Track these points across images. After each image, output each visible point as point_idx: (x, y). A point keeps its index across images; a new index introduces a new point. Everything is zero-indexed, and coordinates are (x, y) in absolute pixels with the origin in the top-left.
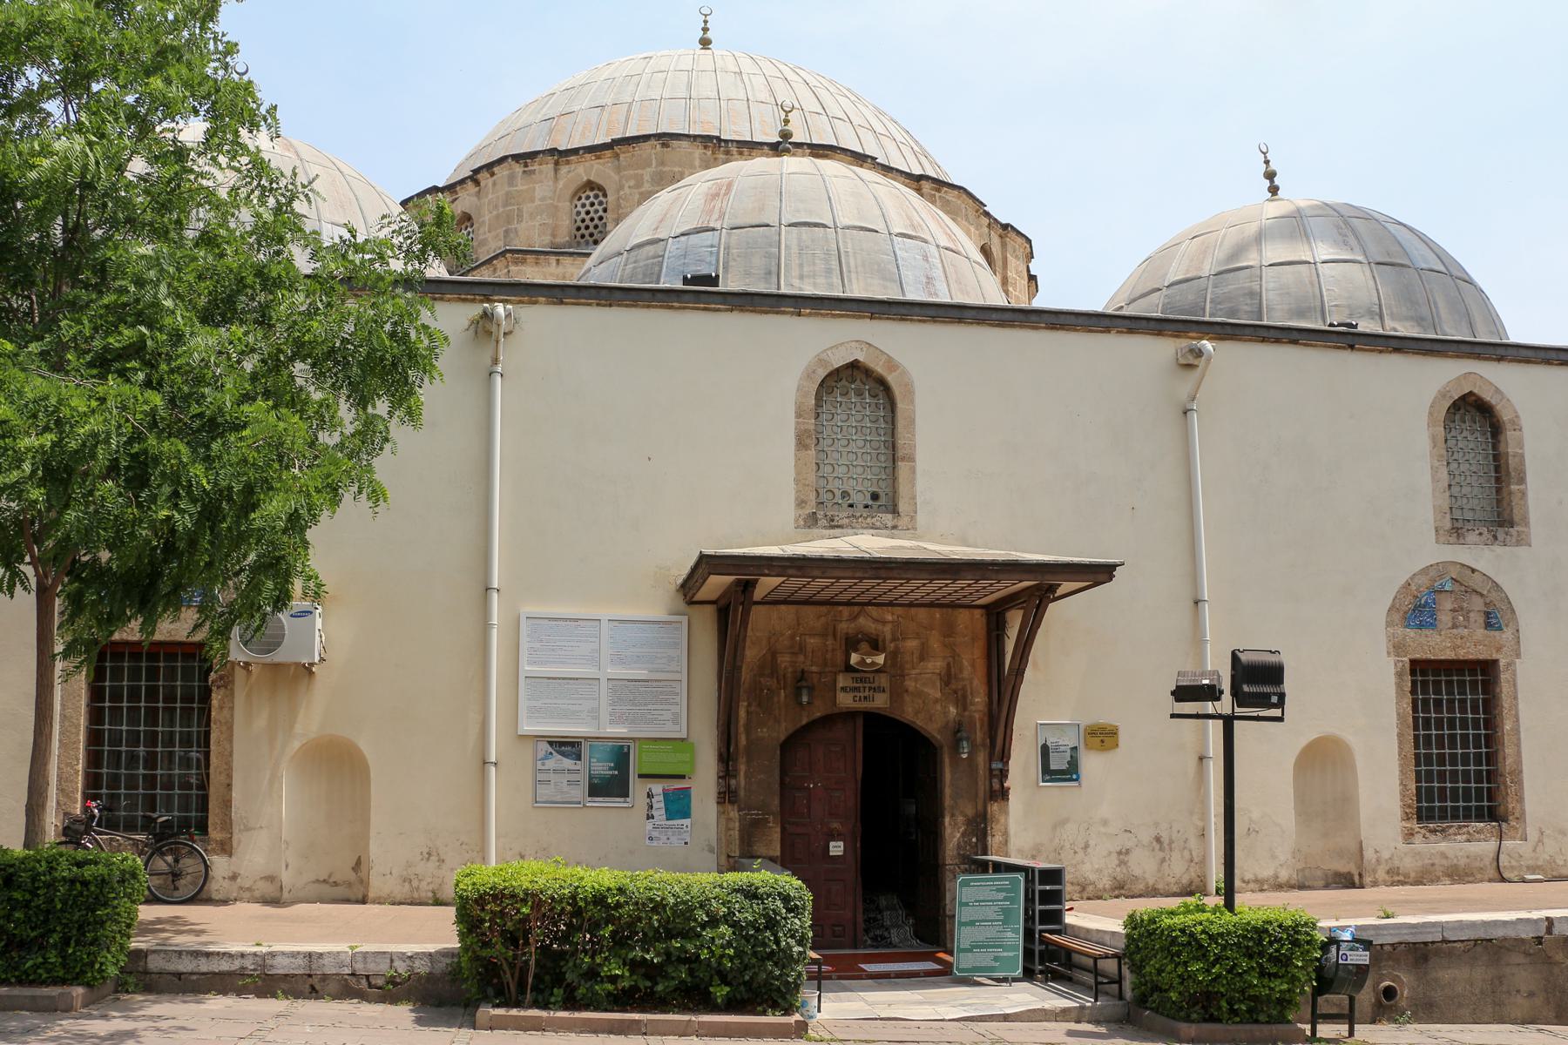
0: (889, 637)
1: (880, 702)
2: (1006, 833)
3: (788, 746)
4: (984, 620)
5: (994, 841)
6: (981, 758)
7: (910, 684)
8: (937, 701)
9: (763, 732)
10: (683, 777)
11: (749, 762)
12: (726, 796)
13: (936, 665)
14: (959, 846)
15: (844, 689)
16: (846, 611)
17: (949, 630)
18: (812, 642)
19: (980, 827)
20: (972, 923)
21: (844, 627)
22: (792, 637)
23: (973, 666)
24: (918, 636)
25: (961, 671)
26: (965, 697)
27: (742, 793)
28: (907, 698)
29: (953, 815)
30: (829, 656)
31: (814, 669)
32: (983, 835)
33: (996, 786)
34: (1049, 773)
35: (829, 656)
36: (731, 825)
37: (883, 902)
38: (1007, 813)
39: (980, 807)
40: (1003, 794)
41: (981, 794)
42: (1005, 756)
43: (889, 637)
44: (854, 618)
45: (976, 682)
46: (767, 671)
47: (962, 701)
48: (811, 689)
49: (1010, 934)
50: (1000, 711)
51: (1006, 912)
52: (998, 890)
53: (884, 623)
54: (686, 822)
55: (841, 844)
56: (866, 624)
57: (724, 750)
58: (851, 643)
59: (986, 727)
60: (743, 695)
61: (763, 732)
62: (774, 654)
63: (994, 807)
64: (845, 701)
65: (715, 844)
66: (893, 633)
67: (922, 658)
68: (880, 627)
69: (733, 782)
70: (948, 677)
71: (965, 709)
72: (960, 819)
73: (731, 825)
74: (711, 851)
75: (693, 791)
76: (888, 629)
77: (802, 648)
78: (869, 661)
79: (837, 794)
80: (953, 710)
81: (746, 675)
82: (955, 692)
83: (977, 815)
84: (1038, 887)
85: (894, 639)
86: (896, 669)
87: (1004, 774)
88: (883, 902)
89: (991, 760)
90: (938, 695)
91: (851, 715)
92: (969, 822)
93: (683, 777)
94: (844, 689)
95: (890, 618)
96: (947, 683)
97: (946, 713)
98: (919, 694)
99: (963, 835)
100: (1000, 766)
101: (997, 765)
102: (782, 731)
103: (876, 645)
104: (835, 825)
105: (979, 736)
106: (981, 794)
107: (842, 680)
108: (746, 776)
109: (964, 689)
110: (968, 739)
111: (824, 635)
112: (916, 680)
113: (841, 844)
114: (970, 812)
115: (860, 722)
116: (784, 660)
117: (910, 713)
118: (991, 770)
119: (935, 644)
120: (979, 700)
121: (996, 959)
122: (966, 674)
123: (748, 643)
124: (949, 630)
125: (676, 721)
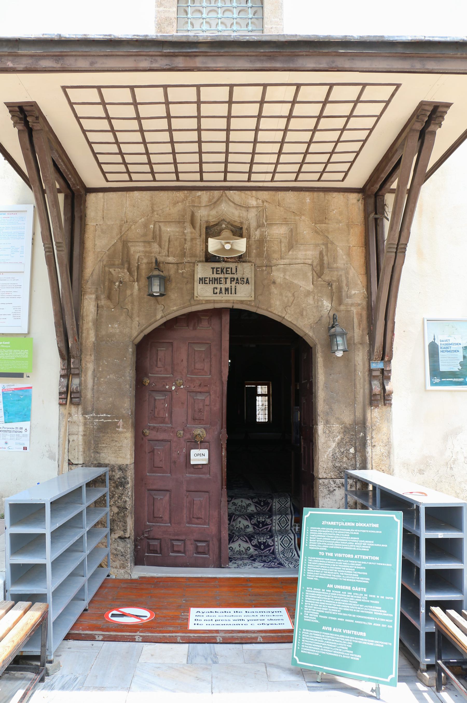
0: (253, 224)
1: (243, 296)
2: (388, 444)
3: (145, 346)
4: (360, 205)
5: (374, 453)
6: (360, 357)
7: (278, 275)
8: (308, 294)
9: (114, 328)
10: (20, 375)
11: (98, 360)
12: (69, 397)
13: (307, 254)
14: (334, 458)
15: (202, 280)
16: (204, 196)
17: (321, 216)
18: (169, 230)
19: (358, 438)
20: (321, 584)
21: (204, 214)
22: (146, 225)
23: (349, 255)
24: (285, 221)
25: (335, 259)
26: (340, 289)
27: (89, 394)
28: (274, 290)
29: (327, 422)
30: (187, 246)
31: (171, 259)
32: (362, 445)
33: (377, 388)
34: (438, 375)
35: (187, 246)
36: (74, 429)
37: (276, 504)
38: (389, 420)
39: (359, 414)
40: (385, 398)
41: (360, 398)
42: (385, 354)
43: (253, 224)
44: (214, 204)
45: (352, 272)
46: (118, 261)
47: (337, 293)
48: (165, 281)
49: (378, 610)
50: (378, 298)
51: (373, 572)
52: (363, 537)
53: (248, 208)
54: (25, 425)
55: (206, 452)
56: (228, 210)
57: (63, 345)
58: (212, 230)
59: (365, 322)
60: (89, 287)
61: (114, 328)
62: (125, 243)
63: (374, 414)
64: (205, 295)
65: (55, 449)
66: (258, 218)
67: (291, 247)
68: (244, 213)
69: (75, 382)
70: (320, 268)
71: (340, 302)
72: (336, 427)
73: (74, 429)
74: (52, 457)
75: (34, 393)
76: (252, 214)
77: (157, 237)
78: (228, 247)
79: (200, 397)
80: (327, 304)
81: (92, 265)
82: (330, 284)
83: (355, 423)
84: (425, 534)
85: (259, 226)
86: (260, 253)
87: (385, 375)
88: (276, 504)
89: (370, 360)
90: (310, 287)
91: (216, 313)
92: (346, 430)
93: (20, 375)
94: (202, 280)
95: (253, 202)
96: (320, 275)
97: (319, 307)
98: (289, 286)
99: (339, 445)
100: (380, 365)
101: (377, 365)
102: (134, 327)
103: (238, 232)
104: (199, 431)
105: (358, 333)
106: (360, 398)
107: (203, 270)
108: (94, 376)
109: (339, 281)
110: (343, 335)
111: (180, 222)
112: (285, 271)
113: (206, 452)
114: (348, 419)
115: (226, 319)
116: (137, 250)
117: (278, 308)
118: (370, 371)
119: (305, 229)
120: (356, 293)
121: (355, 648)
122: (341, 263)
123: (295, 322)
124: (321, 216)
125: (16, 316)
